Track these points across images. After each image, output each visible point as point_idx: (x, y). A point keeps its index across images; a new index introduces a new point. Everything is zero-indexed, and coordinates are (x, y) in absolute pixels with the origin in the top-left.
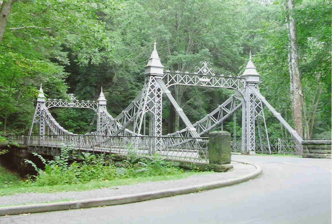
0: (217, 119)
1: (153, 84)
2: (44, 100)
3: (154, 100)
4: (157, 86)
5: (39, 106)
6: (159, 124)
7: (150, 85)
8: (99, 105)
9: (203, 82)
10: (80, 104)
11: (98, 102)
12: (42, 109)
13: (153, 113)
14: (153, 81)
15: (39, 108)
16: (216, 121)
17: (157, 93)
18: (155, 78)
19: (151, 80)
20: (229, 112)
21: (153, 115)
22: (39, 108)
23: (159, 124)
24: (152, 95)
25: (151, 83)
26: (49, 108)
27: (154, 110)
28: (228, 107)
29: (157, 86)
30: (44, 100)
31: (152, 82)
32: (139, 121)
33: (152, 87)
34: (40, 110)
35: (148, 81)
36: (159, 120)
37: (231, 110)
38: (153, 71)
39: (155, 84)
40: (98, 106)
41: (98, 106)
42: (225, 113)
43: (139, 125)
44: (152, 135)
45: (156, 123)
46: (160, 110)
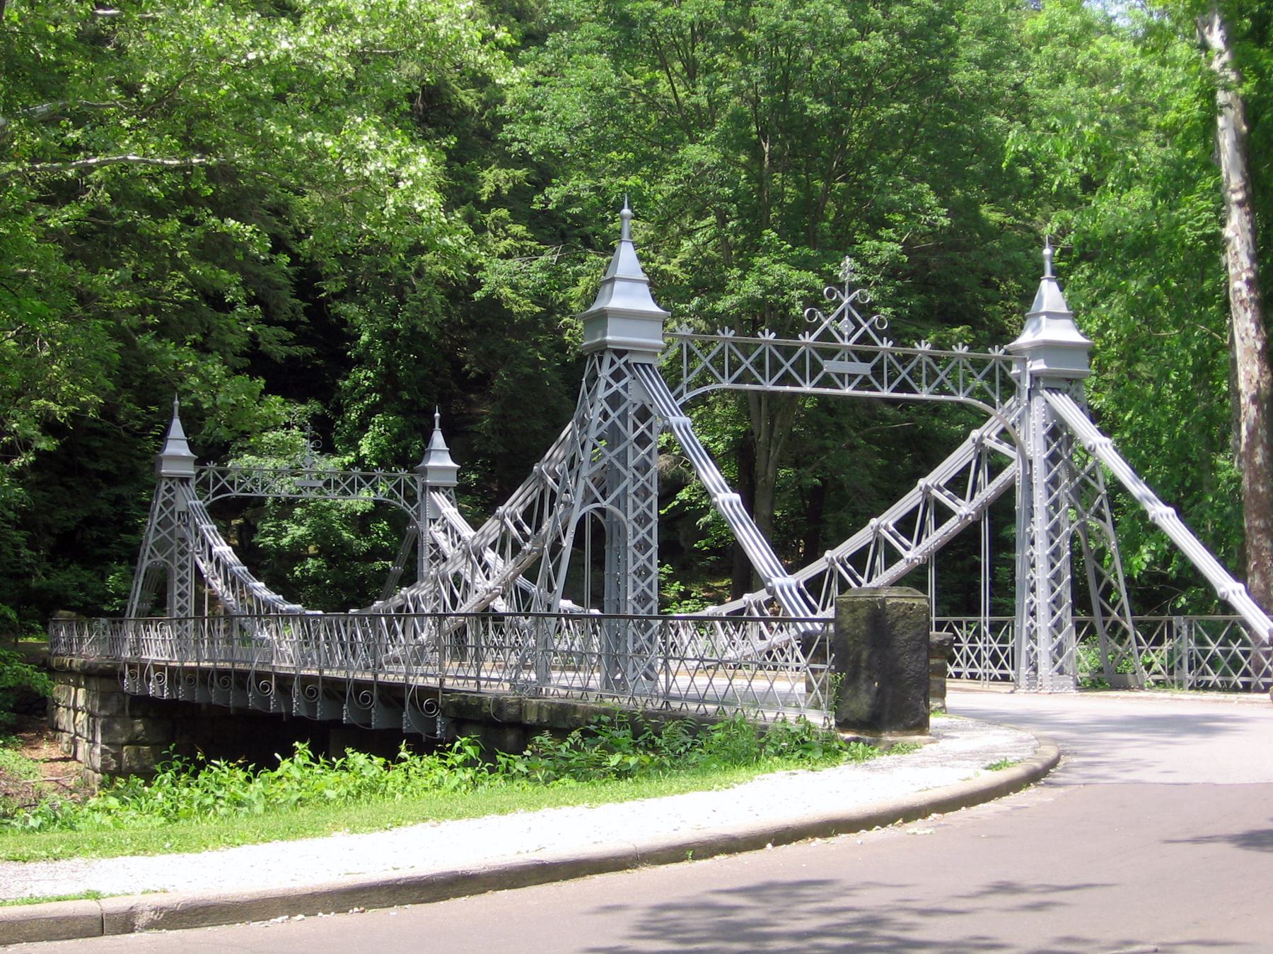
0: (910, 538)
1: (616, 386)
2: (190, 470)
3: (623, 458)
4: (634, 397)
5: (169, 496)
6: (647, 512)
7: (602, 394)
8: (424, 486)
9: (841, 376)
10: (223, 481)
11: (424, 472)
12: (180, 506)
13: (622, 516)
14: (617, 376)
15: (167, 504)
16: (907, 549)
17: (636, 427)
18: (626, 363)
19: (605, 373)
20: (964, 509)
21: (621, 530)
22: (167, 504)
23: (647, 512)
24: (614, 437)
25: (609, 385)
26: (212, 500)
27: (171, 557)
28: (958, 485)
29: (634, 397)
30: (190, 470)
31: (612, 381)
32: (556, 548)
33: (615, 400)
34: (172, 513)
35: (594, 378)
36: (643, 546)
37: (972, 498)
38: (614, 335)
39: (625, 387)
40: (419, 490)
41: (419, 490)
42: (943, 514)
43: (556, 569)
44: (618, 609)
45: (633, 561)
46: (649, 580)
